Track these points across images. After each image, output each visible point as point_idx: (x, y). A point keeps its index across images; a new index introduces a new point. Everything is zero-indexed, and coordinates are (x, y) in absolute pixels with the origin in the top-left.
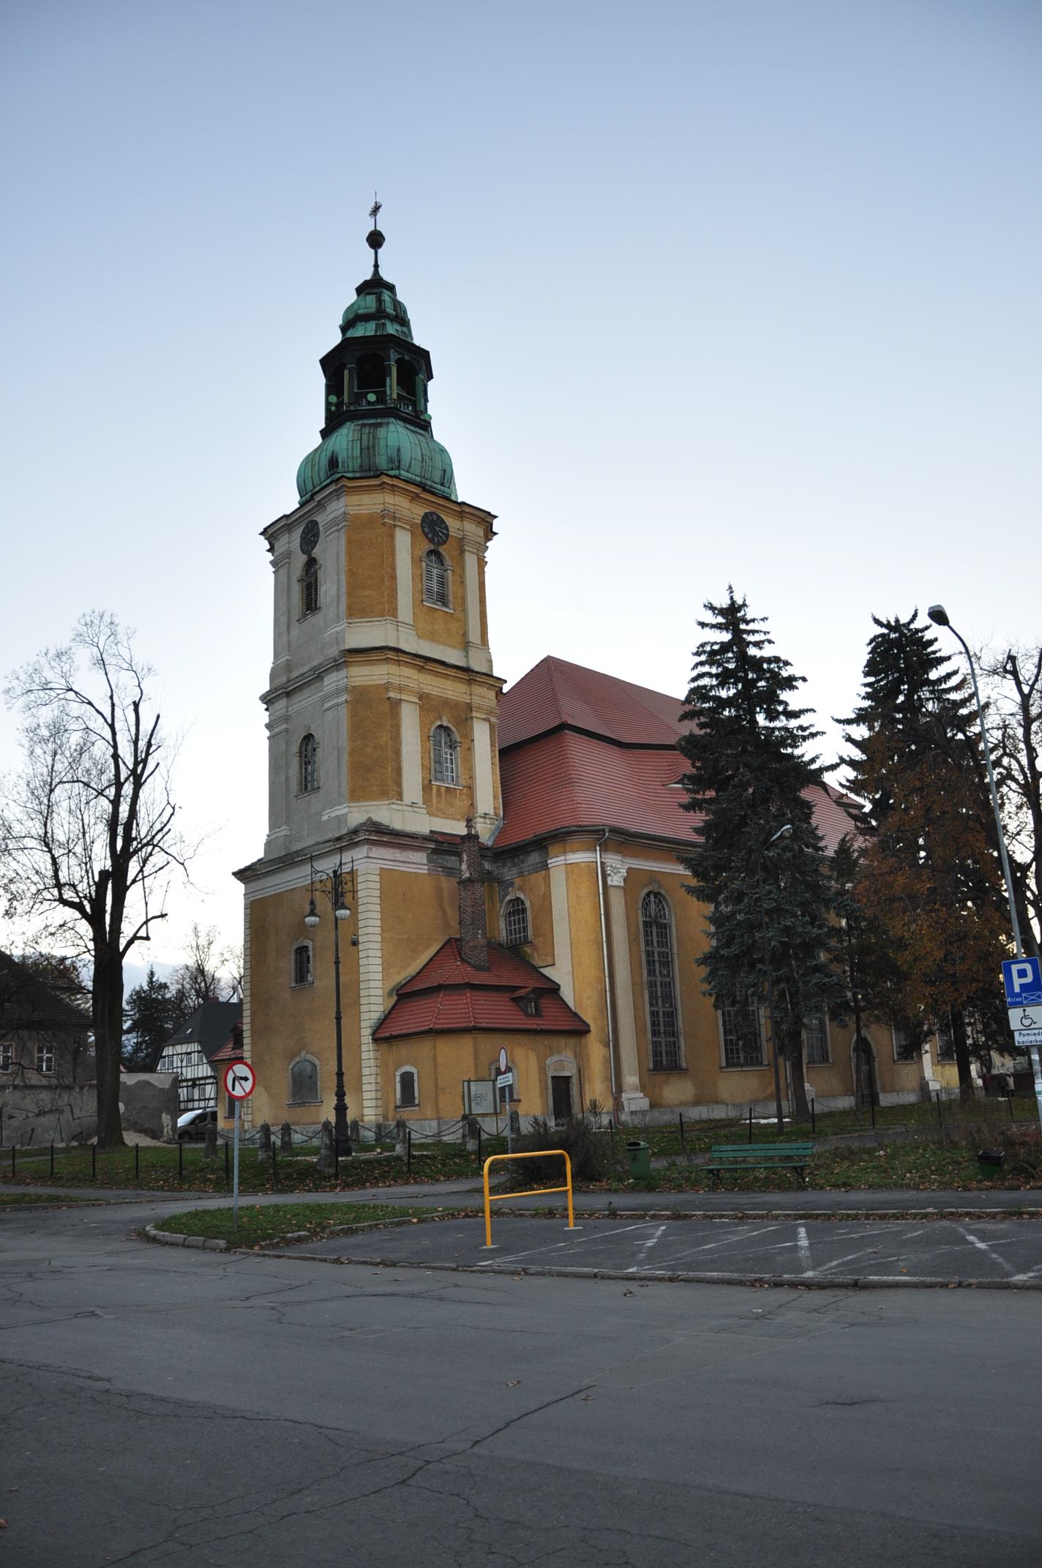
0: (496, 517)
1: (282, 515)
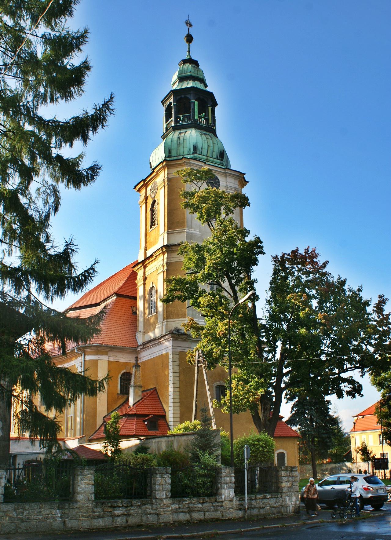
0: (245, 174)
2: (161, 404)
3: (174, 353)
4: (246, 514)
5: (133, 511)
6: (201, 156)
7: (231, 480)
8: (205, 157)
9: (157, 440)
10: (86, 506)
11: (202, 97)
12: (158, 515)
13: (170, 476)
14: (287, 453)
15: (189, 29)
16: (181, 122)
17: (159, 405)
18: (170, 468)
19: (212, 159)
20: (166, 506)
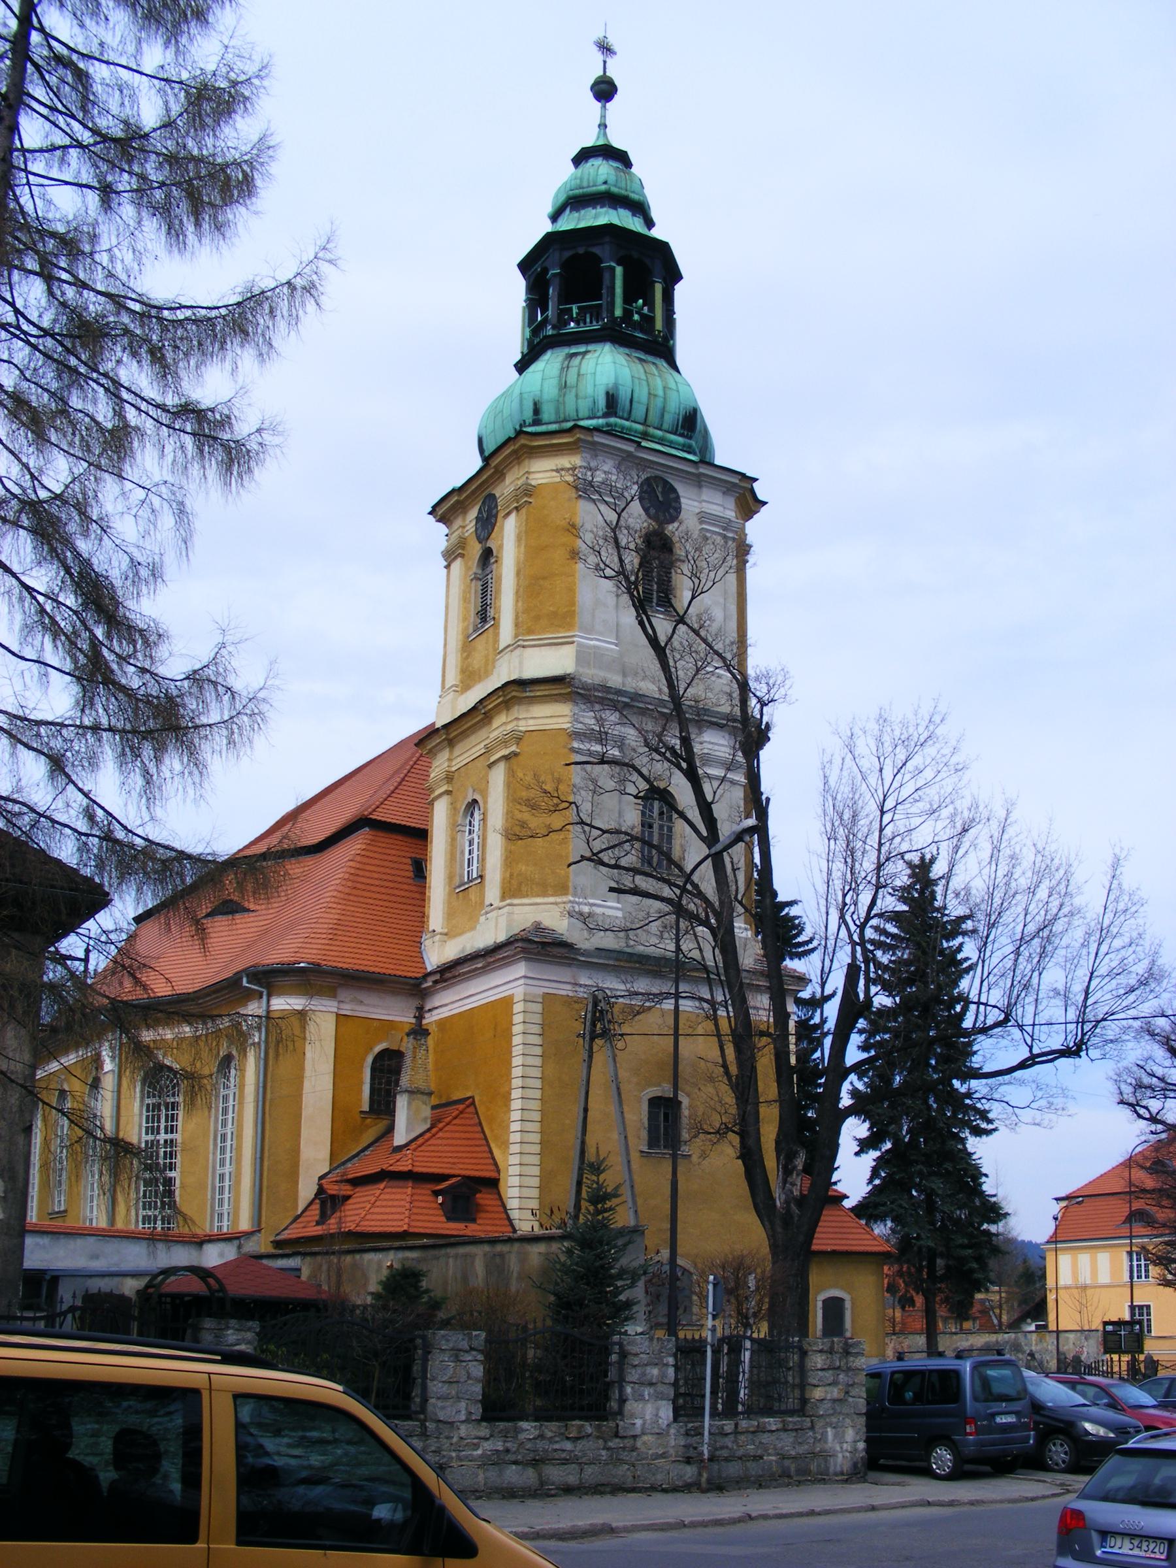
0: (755, 480)
1: (450, 489)
2: (489, 1145)
3: (528, 998)
4: (705, 1475)
6: (627, 423)
7: (663, 1375)
8: (640, 427)
9: (462, 1250)
11: (635, 255)
13: (480, 1357)
14: (853, 1301)
15: (605, 62)
16: (572, 324)
17: (483, 1149)
18: (484, 1335)
19: (659, 433)
20: (467, 1445)
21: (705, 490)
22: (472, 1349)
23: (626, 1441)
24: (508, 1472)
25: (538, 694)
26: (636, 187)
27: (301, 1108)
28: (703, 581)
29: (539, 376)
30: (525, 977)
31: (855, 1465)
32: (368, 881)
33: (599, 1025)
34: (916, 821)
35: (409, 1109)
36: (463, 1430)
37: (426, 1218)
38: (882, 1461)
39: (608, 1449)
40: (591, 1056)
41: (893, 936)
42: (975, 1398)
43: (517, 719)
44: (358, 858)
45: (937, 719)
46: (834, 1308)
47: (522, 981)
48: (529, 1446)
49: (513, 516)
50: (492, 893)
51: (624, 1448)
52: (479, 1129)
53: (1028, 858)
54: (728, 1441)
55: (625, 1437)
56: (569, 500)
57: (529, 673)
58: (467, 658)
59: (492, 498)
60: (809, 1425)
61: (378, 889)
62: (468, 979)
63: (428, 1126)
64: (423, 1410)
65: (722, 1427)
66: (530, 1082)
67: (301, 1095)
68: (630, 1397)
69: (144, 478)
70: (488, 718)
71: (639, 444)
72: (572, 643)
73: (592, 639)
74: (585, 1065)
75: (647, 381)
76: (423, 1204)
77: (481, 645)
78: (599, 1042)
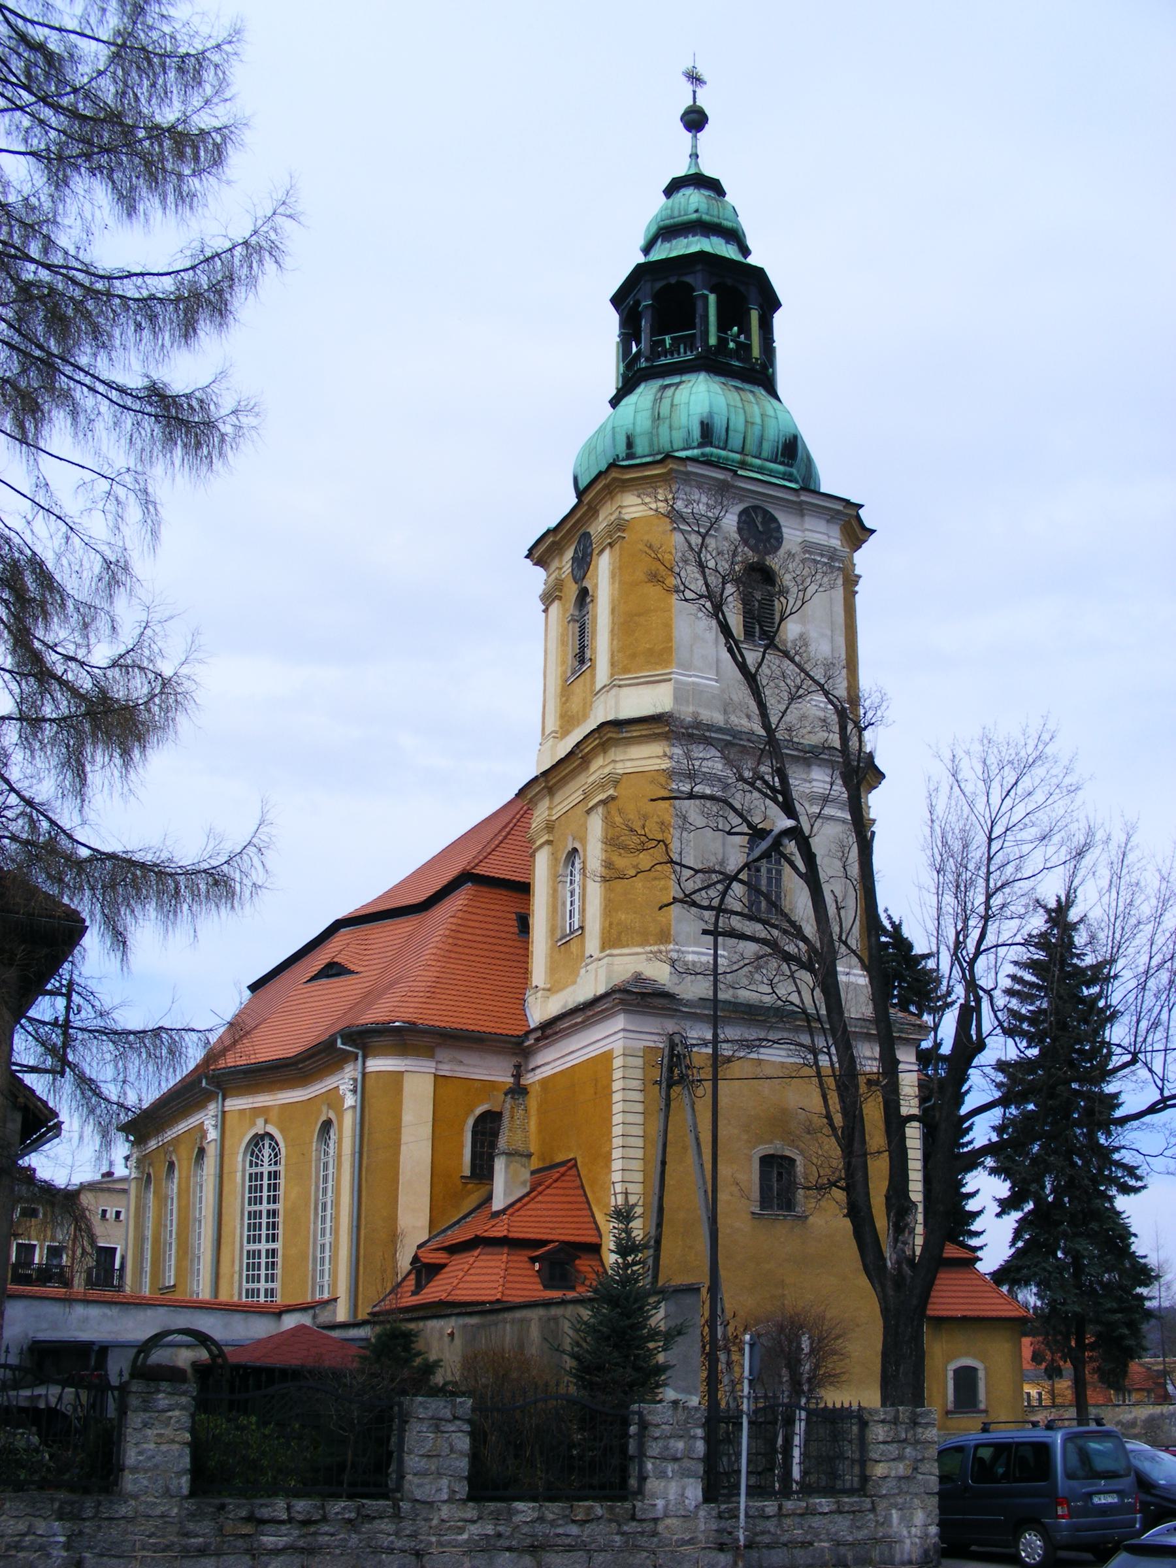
0: (861, 506)
1: (544, 530)
3: (627, 1052)
5: (327, 1538)
6: (723, 453)
8: (737, 456)
9: (518, 1314)
10: (158, 1512)
11: (729, 282)
12: (418, 1554)
13: (467, 1428)
14: (986, 1369)
15: (694, 92)
17: (584, 1213)
19: (758, 462)
20: (449, 1528)
21: (807, 518)
22: (455, 1418)
23: (644, 1525)
24: (500, 1560)
25: (635, 734)
26: (730, 213)
27: (397, 1174)
28: (791, 602)
29: (631, 409)
30: (624, 1030)
31: (926, 1552)
32: (470, 937)
33: (676, 1071)
34: (1026, 848)
35: (506, 1172)
36: (445, 1511)
37: (524, 1286)
38: (973, 1548)
39: (623, 1534)
40: (668, 1105)
41: (1032, 985)
42: (1070, 1476)
43: (614, 761)
44: (460, 914)
45: (1046, 737)
46: (966, 1380)
47: (621, 1035)
48: (525, 1529)
49: (607, 552)
50: (592, 944)
51: (642, 1533)
52: (581, 1192)
53: (1151, 882)
54: (771, 1525)
55: (644, 1520)
56: (664, 532)
57: (626, 713)
58: (565, 703)
59: (587, 535)
60: (869, 1506)
61: (481, 946)
62: (568, 1035)
63: (527, 1189)
64: (399, 1488)
65: (763, 1509)
66: (632, 1141)
67: (397, 1162)
68: (651, 1474)
69: (106, 466)
70: (585, 762)
71: (735, 472)
72: (670, 680)
73: (690, 676)
74: (662, 1114)
75: (744, 409)
76: (518, 1272)
77: (579, 688)
78: (676, 1089)
